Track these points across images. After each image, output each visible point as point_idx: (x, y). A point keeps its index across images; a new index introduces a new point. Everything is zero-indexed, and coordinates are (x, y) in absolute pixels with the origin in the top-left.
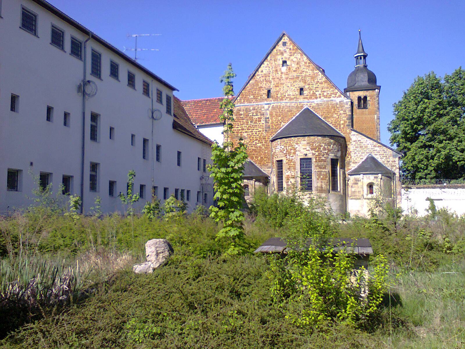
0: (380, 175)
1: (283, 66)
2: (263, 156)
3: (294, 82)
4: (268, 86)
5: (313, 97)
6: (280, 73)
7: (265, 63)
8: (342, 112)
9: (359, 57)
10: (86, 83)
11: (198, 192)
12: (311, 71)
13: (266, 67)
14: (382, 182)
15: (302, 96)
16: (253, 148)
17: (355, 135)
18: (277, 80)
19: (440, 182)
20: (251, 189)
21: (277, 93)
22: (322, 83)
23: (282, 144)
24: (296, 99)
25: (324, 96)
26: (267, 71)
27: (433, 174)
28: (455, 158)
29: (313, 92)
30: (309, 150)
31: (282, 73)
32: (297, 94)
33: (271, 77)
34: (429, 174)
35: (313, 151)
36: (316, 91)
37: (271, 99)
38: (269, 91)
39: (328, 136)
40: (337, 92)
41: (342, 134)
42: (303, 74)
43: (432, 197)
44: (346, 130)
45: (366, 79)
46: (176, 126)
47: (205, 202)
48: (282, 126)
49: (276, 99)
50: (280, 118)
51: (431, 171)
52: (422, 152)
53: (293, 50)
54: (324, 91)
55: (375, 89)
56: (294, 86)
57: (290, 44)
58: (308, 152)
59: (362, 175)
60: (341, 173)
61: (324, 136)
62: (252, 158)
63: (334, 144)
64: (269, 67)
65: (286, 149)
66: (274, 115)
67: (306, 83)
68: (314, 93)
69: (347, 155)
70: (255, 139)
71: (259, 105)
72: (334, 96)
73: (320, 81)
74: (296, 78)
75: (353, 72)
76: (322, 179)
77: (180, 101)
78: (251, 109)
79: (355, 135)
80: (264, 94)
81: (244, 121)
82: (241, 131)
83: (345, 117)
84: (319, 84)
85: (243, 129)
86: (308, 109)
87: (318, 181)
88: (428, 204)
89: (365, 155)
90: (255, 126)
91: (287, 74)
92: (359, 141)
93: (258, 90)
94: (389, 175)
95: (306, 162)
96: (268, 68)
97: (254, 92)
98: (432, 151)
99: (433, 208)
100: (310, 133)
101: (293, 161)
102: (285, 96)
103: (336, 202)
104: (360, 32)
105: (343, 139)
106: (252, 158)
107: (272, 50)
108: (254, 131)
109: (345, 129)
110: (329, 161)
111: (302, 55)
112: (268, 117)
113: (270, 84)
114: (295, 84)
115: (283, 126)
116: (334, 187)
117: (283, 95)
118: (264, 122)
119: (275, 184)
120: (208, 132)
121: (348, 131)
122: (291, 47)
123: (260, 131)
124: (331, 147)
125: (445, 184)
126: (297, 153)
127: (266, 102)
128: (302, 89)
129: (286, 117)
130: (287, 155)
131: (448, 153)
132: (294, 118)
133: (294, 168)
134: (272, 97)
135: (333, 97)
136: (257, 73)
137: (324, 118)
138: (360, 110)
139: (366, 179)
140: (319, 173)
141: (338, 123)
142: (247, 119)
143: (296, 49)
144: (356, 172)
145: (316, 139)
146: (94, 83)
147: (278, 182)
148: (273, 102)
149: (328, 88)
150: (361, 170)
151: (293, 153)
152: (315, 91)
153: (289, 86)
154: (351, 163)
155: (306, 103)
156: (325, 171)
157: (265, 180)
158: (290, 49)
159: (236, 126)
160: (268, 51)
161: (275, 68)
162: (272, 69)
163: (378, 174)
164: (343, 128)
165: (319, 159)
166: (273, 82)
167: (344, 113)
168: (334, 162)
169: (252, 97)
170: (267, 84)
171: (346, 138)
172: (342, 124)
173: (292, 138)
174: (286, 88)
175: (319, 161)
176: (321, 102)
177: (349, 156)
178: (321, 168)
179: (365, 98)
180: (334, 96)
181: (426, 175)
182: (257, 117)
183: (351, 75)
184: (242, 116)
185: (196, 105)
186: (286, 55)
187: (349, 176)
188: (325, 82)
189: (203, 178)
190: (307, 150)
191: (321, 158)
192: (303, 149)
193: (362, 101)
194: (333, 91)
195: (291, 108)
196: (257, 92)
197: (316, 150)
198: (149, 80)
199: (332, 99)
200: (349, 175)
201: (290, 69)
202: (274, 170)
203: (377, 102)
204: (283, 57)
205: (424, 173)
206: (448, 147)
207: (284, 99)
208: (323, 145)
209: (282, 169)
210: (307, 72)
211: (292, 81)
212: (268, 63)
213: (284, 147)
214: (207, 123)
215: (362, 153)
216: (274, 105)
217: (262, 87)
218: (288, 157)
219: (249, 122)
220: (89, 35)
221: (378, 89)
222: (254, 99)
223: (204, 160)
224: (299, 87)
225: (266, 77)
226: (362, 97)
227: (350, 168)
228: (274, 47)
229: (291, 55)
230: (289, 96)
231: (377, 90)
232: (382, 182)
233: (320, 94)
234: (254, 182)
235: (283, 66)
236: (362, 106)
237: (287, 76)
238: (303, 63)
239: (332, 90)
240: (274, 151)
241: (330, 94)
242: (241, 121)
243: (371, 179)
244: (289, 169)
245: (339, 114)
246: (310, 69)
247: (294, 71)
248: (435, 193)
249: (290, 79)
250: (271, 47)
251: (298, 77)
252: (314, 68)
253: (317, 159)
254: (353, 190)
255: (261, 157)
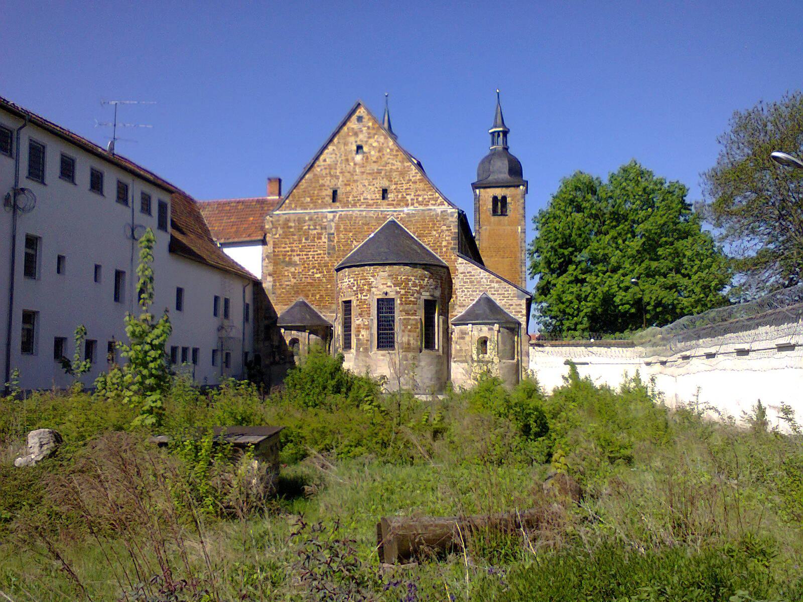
1: (357, 152)
2: (323, 293)
5: (402, 204)
6: (352, 164)
8: (444, 228)
9: (496, 134)
10: (18, 191)
11: (214, 351)
12: (400, 164)
13: (331, 154)
14: (499, 338)
15: (386, 202)
16: (309, 280)
18: (348, 175)
19: (599, 338)
20: (302, 347)
21: (348, 194)
22: (415, 182)
25: (418, 202)
26: (332, 160)
27: (586, 323)
28: (617, 300)
30: (391, 287)
32: (378, 197)
35: (398, 288)
37: (338, 204)
38: (335, 193)
39: (420, 264)
41: (444, 261)
43: (574, 360)
44: (450, 256)
45: (506, 170)
46: (176, 248)
47: (227, 366)
49: (346, 204)
50: (351, 234)
52: (571, 290)
54: (418, 195)
55: (518, 186)
57: (369, 120)
58: (388, 290)
60: (441, 321)
61: (414, 265)
63: (430, 278)
66: (341, 229)
68: (403, 197)
72: (434, 202)
73: (413, 179)
74: (377, 173)
75: (487, 157)
76: (410, 331)
77: (195, 202)
81: (295, 237)
82: (290, 253)
84: (411, 183)
85: (292, 251)
88: (566, 371)
89: (477, 294)
91: (363, 167)
92: (468, 273)
93: (319, 190)
94: (512, 328)
96: (333, 156)
97: (312, 192)
98: (587, 289)
99: (574, 374)
100: (393, 259)
102: (360, 200)
103: (432, 367)
104: (498, 93)
105: (445, 270)
110: (422, 303)
111: (386, 138)
112: (332, 231)
114: (375, 182)
115: (355, 247)
116: (429, 343)
119: (341, 337)
120: (237, 254)
121: (453, 257)
122: (370, 124)
123: (320, 254)
124: (426, 281)
125: (592, 340)
126: (373, 289)
128: (385, 192)
129: (360, 232)
131: (607, 291)
132: (372, 235)
134: (340, 201)
137: (417, 237)
138: (496, 218)
139: (476, 332)
140: (405, 322)
141: (438, 244)
144: (462, 321)
146: (30, 191)
147: (345, 335)
149: (424, 190)
150: (471, 317)
151: (368, 290)
152: (405, 194)
154: (456, 307)
155: (390, 212)
157: (326, 332)
158: (369, 128)
160: (334, 130)
162: (340, 157)
163: (493, 324)
164: (446, 252)
167: (447, 230)
168: (429, 306)
171: (450, 268)
172: (445, 246)
175: (406, 304)
178: (408, 314)
179: (504, 198)
180: (434, 202)
181: (576, 324)
182: (315, 232)
183: (483, 162)
184: (292, 230)
185: (221, 209)
186: (361, 136)
187: (453, 327)
188: (421, 181)
189: (222, 328)
192: (383, 284)
193: (499, 204)
194: (432, 195)
195: (368, 219)
196: (316, 192)
197: (402, 287)
198: (127, 179)
201: (367, 158)
202: (339, 315)
203: (522, 206)
204: (358, 139)
205: (573, 322)
206: (607, 283)
208: (413, 278)
209: (350, 314)
210: (393, 164)
211: (370, 178)
212: (335, 148)
214: (236, 240)
215: (473, 291)
216: (343, 213)
217: (324, 186)
219: (304, 239)
220: (25, 120)
221: (523, 185)
222: (312, 203)
223: (227, 301)
225: (331, 169)
226: (499, 198)
228: (344, 124)
229: (369, 138)
231: (521, 187)
232: (499, 338)
233: (412, 200)
234: (307, 334)
235: (357, 152)
236: (499, 211)
237: (363, 170)
238: (388, 150)
240: (340, 285)
243: (485, 331)
244: (360, 315)
246: (398, 160)
247: (375, 162)
248: (578, 353)
250: (339, 123)
251: (379, 172)
253: (403, 300)
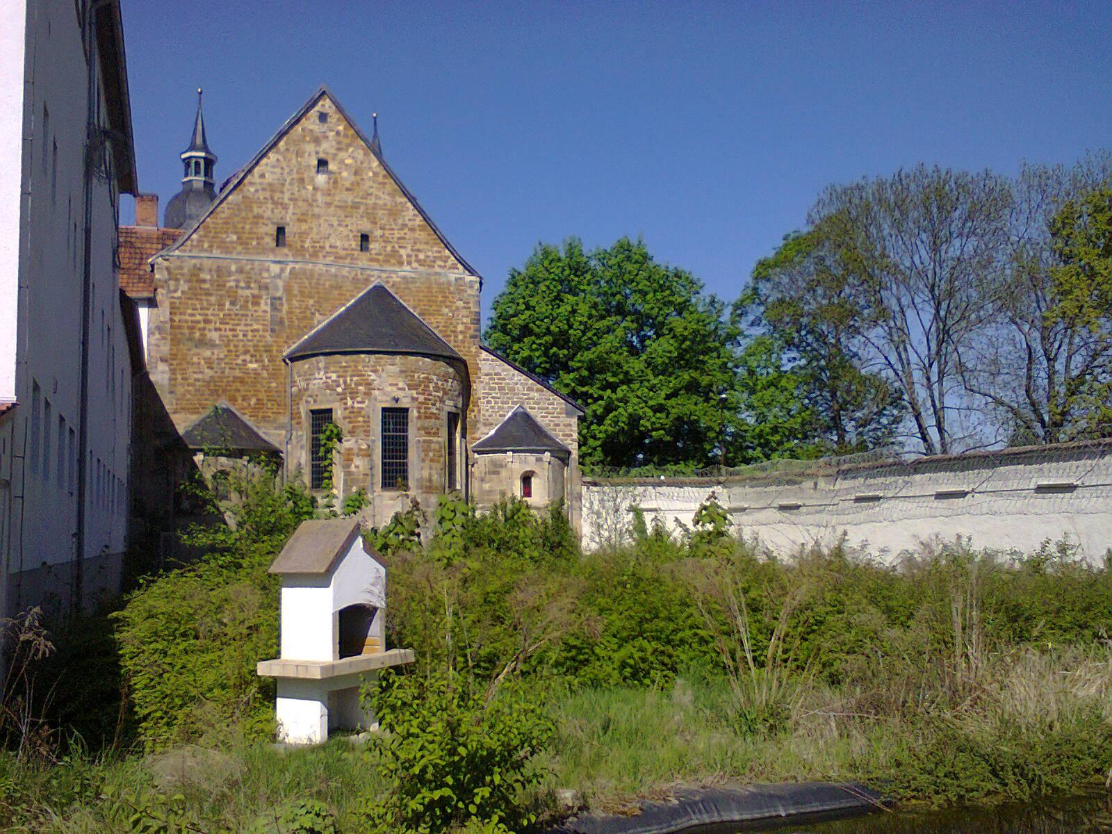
0: (547, 454)
2: (263, 396)
3: (346, 217)
4: (280, 216)
7: (271, 155)
8: (460, 304)
12: (387, 197)
13: (274, 167)
15: (365, 255)
16: (237, 373)
17: (488, 360)
18: (304, 206)
21: (303, 235)
22: (412, 230)
23: (332, 369)
24: (352, 259)
25: (418, 261)
27: (599, 455)
29: (393, 247)
30: (403, 389)
31: (315, 189)
32: (353, 246)
33: (287, 196)
34: (590, 455)
35: (414, 392)
36: (400, 247)
37: (286, 250)
38: (281, 231)
40: (449, 257)
42: (371, 201)
44: (469, 347)
48: (316, 322)
50: (311, 302)
51: (595, 449)
53: (346, 136)
54: (419, 250)
56: (347, 226)
57: (339, 120)
58: (400, 394)
59: (510, 453)
62: (233, 399)
64: (282, 168)
65: (345, 382)
67: (376, 223)
68: (394, 251)
69: (471, 406)
70: (241, 349)
71: (257, 263)
73: (410, 224)
75: (176, 197)
78: (233, 268)
79: (488, 360)
80: (266, 234)
83: (467, 317)
85: (207, 321)
86: (382, 287)
87: (423, 464)
90: (243, 315)
91: (329, 195)
92: (496, 374)
93: (252, 223)
94: (562, 456)
95: (395, 418)
96: (278, 170)
97: (240, 225)
100: (406, 346)
101: (363, 413)
106: (233, 399)
107: (292, 126)
108: (238, 328)
109: (466, 344)
110: (444, 416)
112: (279, 294)
113: (283, 212)
114: (348, 221)
115: (319, 323)
117: (318, 245)
118: (268, 308)
121: (473, 349)
123: (257, 330)
127: (271, 258)
128: (365, 238)
130: (346, 399)
133: (365, 431)
135: (439, 266)
136: (249, 177)
140: (425, 445)
142: (221, 296)
143: (352, 135)
144: (489, 447)
145: (420, 363)
148: (291, 259)
149: (427, 243)
151: (365, 394)
152: (397, 246)
153: (335, 224)
156: (437, 442)
158: (338, 133)
159: (190, 311)
161: (297, 173)
162: (289, 173)
163: (543, 452)
164: (463, 342)
165: (426, 413)
166: (291, 207)
167: (465, 308)
169: (235, 237)
170: (276, 211)
172: (461, 332)
173: (363, 356)
174: (325, 228)
175: (426, 418)
176: (413, 275)
177: (476, 409)
178: (428, 433)
180: (442, 264)
182: (248, 292)
184: (207, 286)
187: (476, 456)
190: (399, 389)
191: (429, 409)
192: (390, 385)
194: (439, 252)
195: (339, 280)
196: (247, 227)
197: (420, 390)
199: (437, 269)
200: (474, 452)
207: (320, 254)
210: (377, 197)
213: (338, 377)
216: (297, 266)
217: (262, 217)
218: (350, 402)
219: (227, 304)
222: (241, 244)
224: (358, 231)
225: (273, 191)
227: (476, 436)
228: (298, 121)
229: (339, 149)
230: (333, 250)
235: (318, 172)
237: (328, 199)
238: (371, 174)
239: (435, 249)
241: (431, 258)
242: (203, 297)
243: (528, 461)
245: (454, 308)
247: (347, 189)
249: (336, 206)
251: (355, 206)
252: (395, 190)
254: (486, 486)
255: (258, 400)
